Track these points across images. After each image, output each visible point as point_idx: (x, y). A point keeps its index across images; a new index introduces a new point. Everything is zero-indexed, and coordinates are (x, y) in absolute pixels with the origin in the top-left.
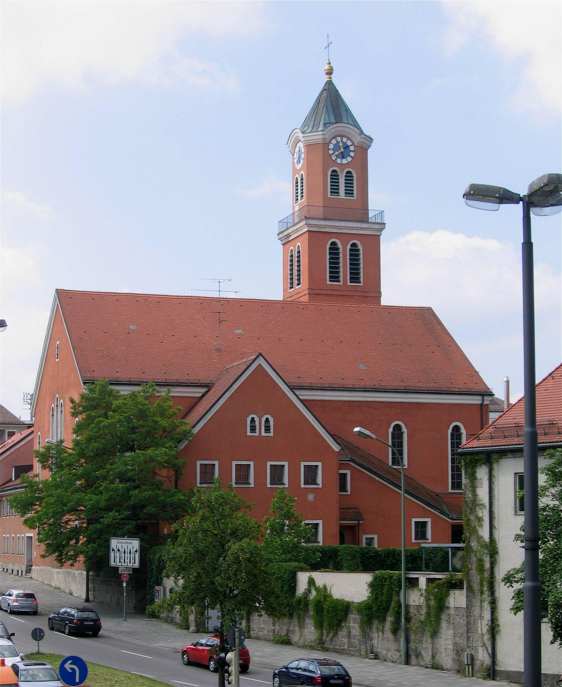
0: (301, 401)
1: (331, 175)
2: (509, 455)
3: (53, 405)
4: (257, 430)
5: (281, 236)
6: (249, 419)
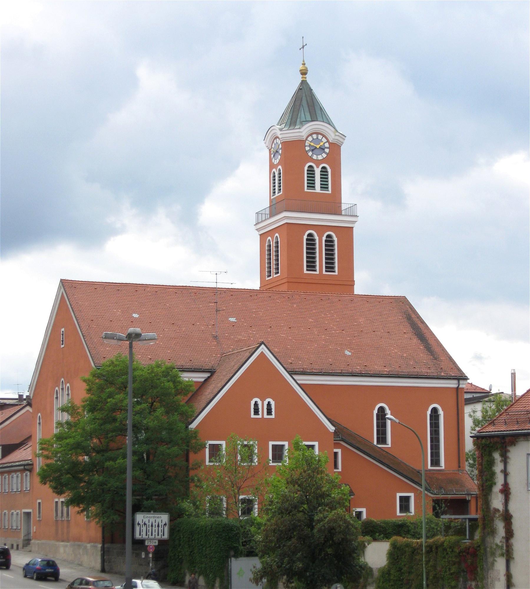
1: (308, 170)
2: (522, 439)
3: (57, 388)
4: (260, 413)
5: (259, 226)
6: (253, 403)
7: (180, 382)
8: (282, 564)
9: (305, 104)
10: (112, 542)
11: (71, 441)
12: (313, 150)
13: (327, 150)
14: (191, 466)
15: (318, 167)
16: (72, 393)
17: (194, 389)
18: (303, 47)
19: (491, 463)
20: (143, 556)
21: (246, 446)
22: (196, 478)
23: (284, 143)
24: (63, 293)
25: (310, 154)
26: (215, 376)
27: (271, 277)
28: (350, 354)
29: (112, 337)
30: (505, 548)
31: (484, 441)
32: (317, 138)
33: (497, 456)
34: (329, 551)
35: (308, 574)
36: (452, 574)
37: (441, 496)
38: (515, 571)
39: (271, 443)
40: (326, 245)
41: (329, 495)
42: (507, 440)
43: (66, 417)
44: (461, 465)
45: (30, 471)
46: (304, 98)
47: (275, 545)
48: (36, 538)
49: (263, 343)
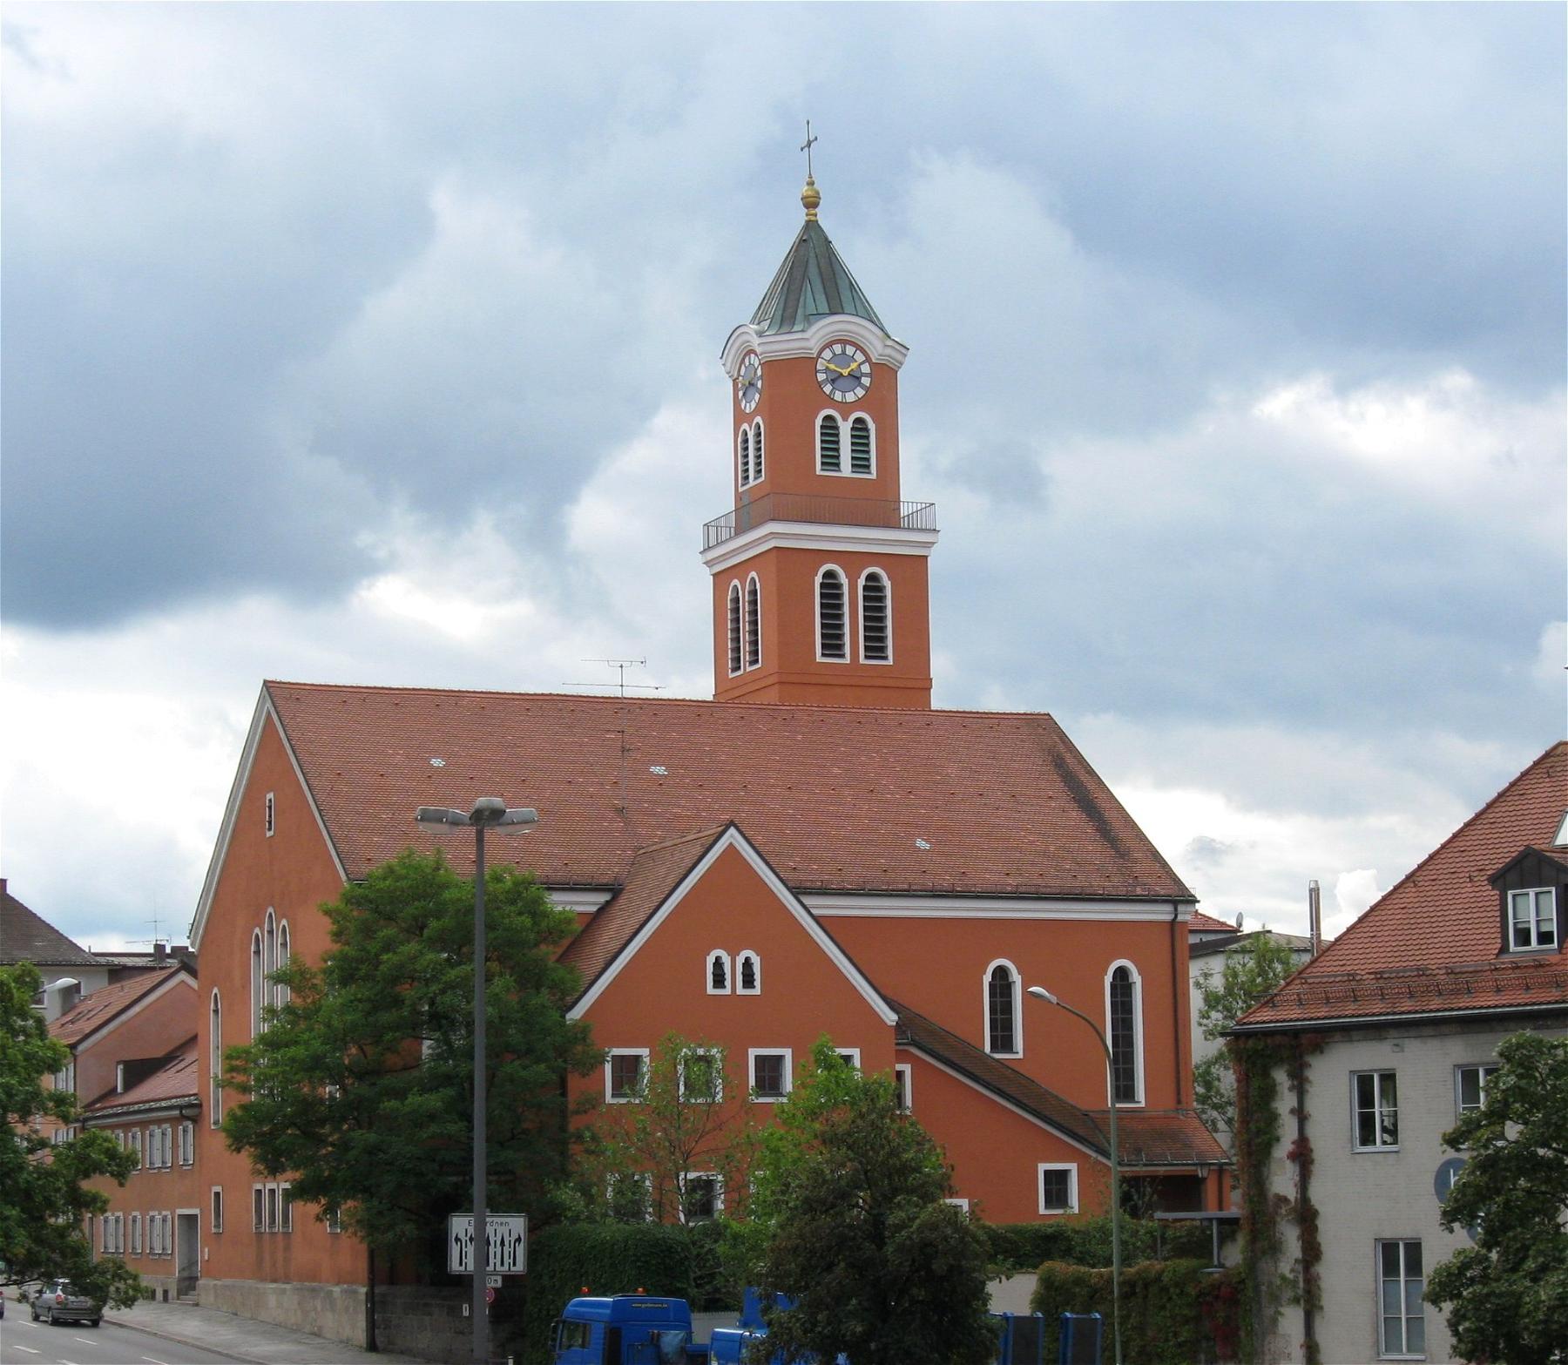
0: (816, 919)
2: (1338, 1037)
3: (257, 930)
4: (728, 983)
6: (710, 960)
7: (545, 915)
8: (814, 1325)
9: (814, 276)
10: (392, 1280)
11: (298, 1052)
12: (833, 381)
13: (866, 381)
14: (571, 1107)
15: (845, 419)
16: (306, 936)
17: (577, 927)
18: (809, 145)
19: (1269, 1092)
20: (466, 1313)
21: (701, 1058)
22: (588, 1134)
23: (768, 365)
24: (269, 713)
25: (828, 389)
26: (622, 900)
27: (741, 672)
28: (928, 846)
29: (437, 818)
30: (1301, 1284)
31: (1251, 1043)
32: (844, 352)
33: (1281, 1077)
34: (920, 1293)
35: (873, 1346)
36: (1180, 1345)
37: (1141, 1170)
38: (1323, 1335)
39: (753, 1053)
40: (865, 598)
41: (918, 1170)
42: (1304, 1039)
43: (282, 996)
44: (1183, 1099)
45: (195, 1120)
46: (812, 261)
47: (796, 1281)
48: (208, 1274)
49: (732, 823)
